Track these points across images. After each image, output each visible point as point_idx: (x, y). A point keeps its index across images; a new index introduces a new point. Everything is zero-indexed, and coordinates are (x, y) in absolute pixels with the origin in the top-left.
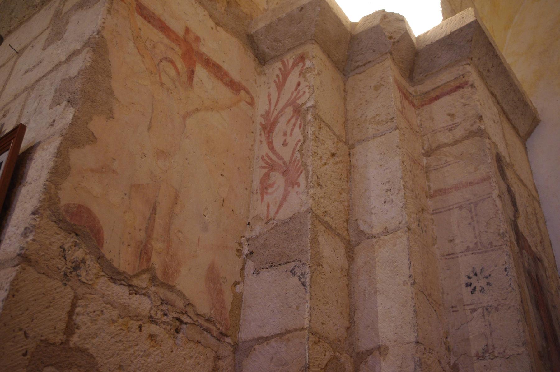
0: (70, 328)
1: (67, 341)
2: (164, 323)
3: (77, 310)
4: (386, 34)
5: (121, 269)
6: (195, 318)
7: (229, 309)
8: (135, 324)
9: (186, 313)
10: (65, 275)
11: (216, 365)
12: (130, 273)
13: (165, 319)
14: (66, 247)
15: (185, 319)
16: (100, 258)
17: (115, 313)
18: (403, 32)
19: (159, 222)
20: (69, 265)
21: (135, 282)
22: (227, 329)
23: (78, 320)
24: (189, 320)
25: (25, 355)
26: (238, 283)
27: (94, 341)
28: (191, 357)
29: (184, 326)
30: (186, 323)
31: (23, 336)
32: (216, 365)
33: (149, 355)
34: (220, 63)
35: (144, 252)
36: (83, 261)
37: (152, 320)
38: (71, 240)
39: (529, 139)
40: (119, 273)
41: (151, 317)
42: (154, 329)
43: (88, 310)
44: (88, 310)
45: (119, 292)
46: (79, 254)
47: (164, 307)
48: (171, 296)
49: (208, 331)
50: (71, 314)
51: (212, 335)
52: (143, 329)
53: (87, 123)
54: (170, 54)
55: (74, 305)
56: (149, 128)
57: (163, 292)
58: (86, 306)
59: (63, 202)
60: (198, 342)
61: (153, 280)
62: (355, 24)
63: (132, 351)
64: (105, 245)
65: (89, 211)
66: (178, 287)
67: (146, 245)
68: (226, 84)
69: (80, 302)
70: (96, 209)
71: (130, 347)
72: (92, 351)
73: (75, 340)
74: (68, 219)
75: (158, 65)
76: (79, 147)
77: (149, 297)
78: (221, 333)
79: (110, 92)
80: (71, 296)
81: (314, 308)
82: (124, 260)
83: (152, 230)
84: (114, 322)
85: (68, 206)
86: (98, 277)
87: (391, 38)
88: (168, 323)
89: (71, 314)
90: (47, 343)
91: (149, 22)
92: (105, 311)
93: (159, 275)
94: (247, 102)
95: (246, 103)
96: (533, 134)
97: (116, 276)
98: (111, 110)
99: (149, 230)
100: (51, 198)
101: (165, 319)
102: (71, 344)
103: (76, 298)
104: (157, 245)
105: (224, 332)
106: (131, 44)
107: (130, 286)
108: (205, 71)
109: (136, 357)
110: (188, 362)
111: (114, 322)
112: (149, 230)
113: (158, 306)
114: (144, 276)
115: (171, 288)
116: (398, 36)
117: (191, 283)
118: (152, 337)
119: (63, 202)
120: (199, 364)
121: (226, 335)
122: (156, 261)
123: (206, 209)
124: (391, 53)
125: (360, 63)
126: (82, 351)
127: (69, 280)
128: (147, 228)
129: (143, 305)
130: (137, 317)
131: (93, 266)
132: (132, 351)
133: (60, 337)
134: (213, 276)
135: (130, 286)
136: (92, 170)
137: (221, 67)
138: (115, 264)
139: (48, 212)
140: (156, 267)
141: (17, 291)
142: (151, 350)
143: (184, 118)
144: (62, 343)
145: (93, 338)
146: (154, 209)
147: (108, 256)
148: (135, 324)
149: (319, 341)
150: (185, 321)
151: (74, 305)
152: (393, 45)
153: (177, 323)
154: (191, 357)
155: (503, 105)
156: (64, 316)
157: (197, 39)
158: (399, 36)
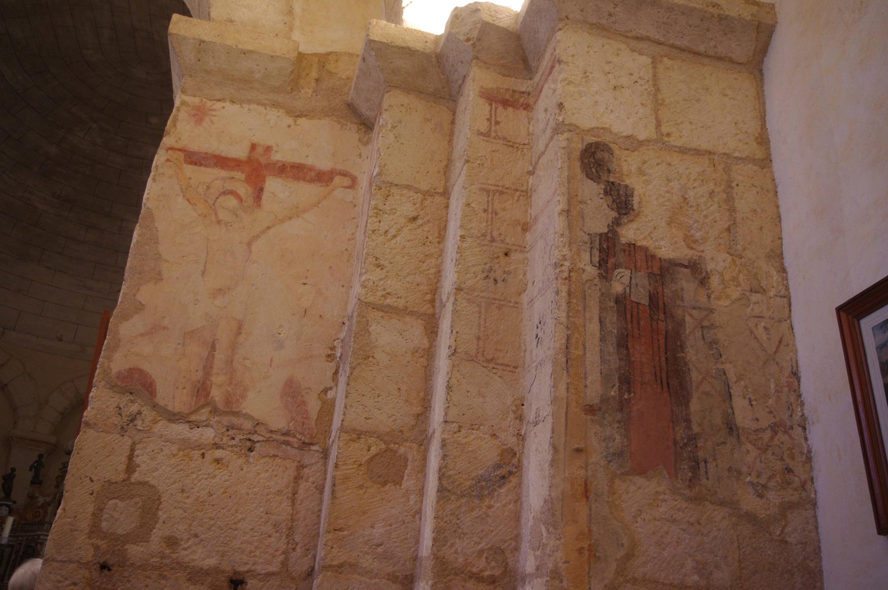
0: (131, 467)
1: (129, 478)
2: (232, 446)
3: (136, 453)
4: (462, 38)
5: (177, 410)
6: (268, 435)
7: (315, 417)
8: (197, 454)
9: (256, 432)
10: (122, 428)
11: (299, 474)
12: (186, 412)
13: (233, 442)
14: (121, 406)
15: (255, 438)
16: (155, 406)
17: (174, 448)
18: (479, 26)
19: (220, 358)
20: (125, 419)
21: (193, 418)
22: (312, 437)
23: (137, 460)
24: (261, 438)
25: (92, 494)
26: (331, 388)
27: (155, 474)
28: (267, 471)
29: (258, 445)
30: (258, 442)
31: (89, 481)
32: (299, 474)
33: (214, 477)
34: (303, 161)
35: (202, 390)
36: (139, 413)
37: (217, 446)
38: (124, 400)
39: (765, 59)
40: (175, 414)
41: (216, 444)
42: (219, 453)
43: (147, 451)
44: (147, 451)
45: (180, 430)
46: (134, 408)
47: (231, 432)
48: (235, 420)
49: (287, 443)
50: (131, 458)
51: (293, 447)
52: (206, 455)
53: (135, 295)
54: (230, 186)
55: (132, 450)
56: (203, 273)
57: (226, 420)
58: (145, 448)
59: (114, 371)
60: (274, 456)
61: (215, 411)
62: (438, 38)
63: (194, 476)
64: (159, 395)
65: (140, 371)
66: (244, 411)
67: (204, 383)
68: (312, 181)
69: (138, 446)
70: (146, 367)
71: (193, 473)
72: (153, 482)
73: (136, 477)
74: (119, 383)
75: (214, 204)
76: (127, 320)
77: (212, 427)
78: (304, 443)
79: (158, 257)
80: (130, 443)
81: (351, 406)
82: (179, 401)
83: (211, 367)
84: (174, 455)
85: (119, 372)
86: (155, 422)
87: (468, 40)
88: (236, 446)
89: (131, 458)
90: (110, 483)
91: (201, 165)
92: (164, 448)
93: (221, 406)
94: (344, 187)
95: (342, 189)
96: (772, 44)
97: (174, 417)
98: (160, 273)
99: (207, 370)
100: (104, 371)
101: (233, 442)
102: (133, 480)
103: (134, 444)
104: (218, 379)
105: (307, 441)
106: (180, 199)
107: (189, 422)
108: (278, 180)
109: (200, 481)
110: (262, 476)
111: (174, 455)
112: (207, 370)
113: (223, 434)
114: (203, 411)
115: (237, 414)
116: (475, 34)
117: (263, 404)
118: (218, 461)
119: (114, 371)
120: (276, 476)
121: (311, 444)
122: (216, 394)
123: (281, 326)
124: (477, 58)
125: (460, 82)
126: (144, 484)
127: (126, 431)
128: (205, 367)
129: (208, 435)
130: (199, 447)
131: (148, 414)
132: (194, 476)
133: (123, 476)
134: (292, 392)
135: (189, 422)
136: (142, 335)
137: (303, 165)
138: (170, 408)
139: (103, 383)
140: (217, 399)
141: (81, 449)
142: (217, 472)
143: (249, 244)
144: (124, 481)
145: (153, 471)
146: (213, 348)
147: (162, 403)
148: (197, 454)
149: (359, 438)
150: (256, 440)
151: (132, 450)
152: (475, 47)
153: (249, 444)
154: (267, 471)
155: (671, 42)
156: (124, 459)
157: (268, 149)
158: (476, 32)
